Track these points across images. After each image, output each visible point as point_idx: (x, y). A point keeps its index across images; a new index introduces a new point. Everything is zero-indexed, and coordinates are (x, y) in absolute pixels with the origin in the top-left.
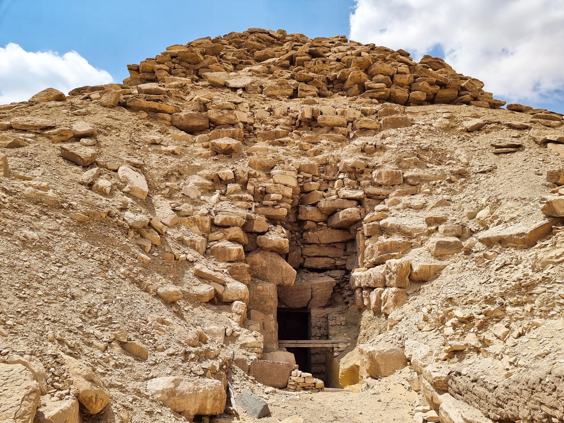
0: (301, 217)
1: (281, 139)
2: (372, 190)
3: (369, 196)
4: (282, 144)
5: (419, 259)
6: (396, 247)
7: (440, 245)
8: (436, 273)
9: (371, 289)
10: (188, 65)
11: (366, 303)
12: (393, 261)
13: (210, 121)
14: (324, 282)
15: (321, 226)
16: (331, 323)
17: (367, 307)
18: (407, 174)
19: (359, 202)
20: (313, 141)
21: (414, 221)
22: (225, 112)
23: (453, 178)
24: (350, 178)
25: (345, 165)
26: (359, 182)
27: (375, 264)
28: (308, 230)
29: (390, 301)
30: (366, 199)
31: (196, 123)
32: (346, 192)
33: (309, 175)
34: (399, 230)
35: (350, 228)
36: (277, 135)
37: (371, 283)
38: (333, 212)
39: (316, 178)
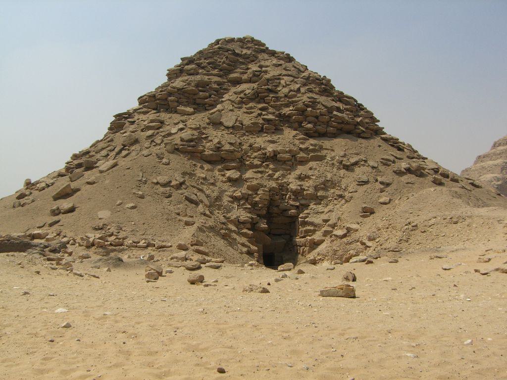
0: (270, 211)
1: (260, 170)
2: (303, 202)
3: (301, 205)
4: (261, 172)
5: (317, 236)
6: (310, 231)
7: (325, 231)
8: (323, 241)
9: (301, 246)
10: (188, 95)
11: (299, 252)
12: (308, 238)
13: (222, 158)
14: (281, 241)
15: (279, 215)
16: (284, 259)
17: (299, 253)
18: (319, 194)
19: (297, 207)
20: (275, 170)
21: (317, 220)
22: (230, 153)
23: (337, 198)
24: (293, 195)
25: (292, 189)
26: (297, 198)
27: (302, 237)
28: (273, 217)
29: (307, 252)
30: (301, 207)
31: (214, 159)
32: (291, 202)
33: (275, 193)
34: (312, 224)
35: (294, 218)
36: (257, 166)
37: (301, 244)
38: (286, 210)
39: (277, 194)
